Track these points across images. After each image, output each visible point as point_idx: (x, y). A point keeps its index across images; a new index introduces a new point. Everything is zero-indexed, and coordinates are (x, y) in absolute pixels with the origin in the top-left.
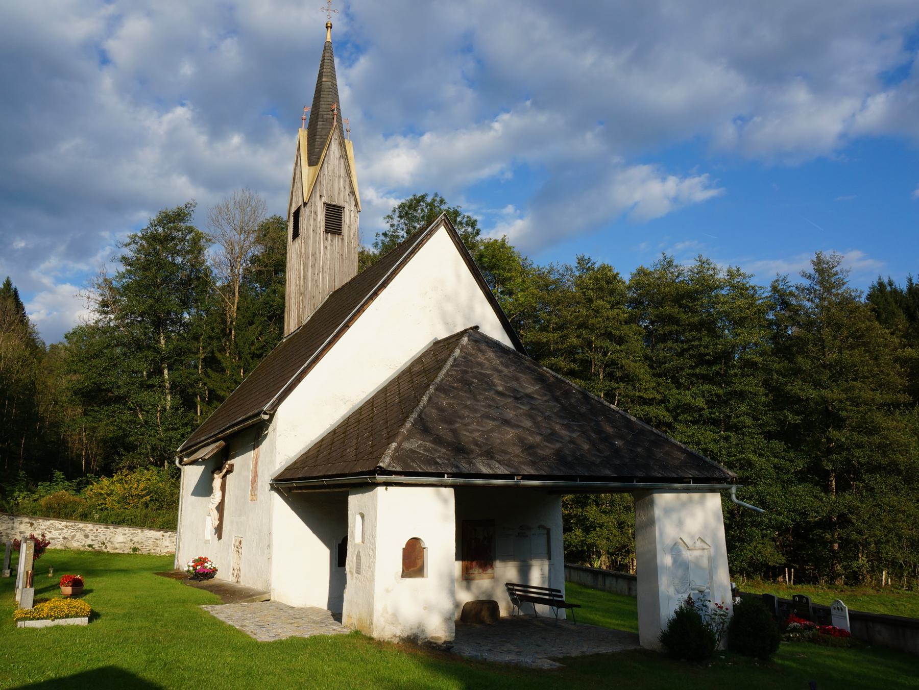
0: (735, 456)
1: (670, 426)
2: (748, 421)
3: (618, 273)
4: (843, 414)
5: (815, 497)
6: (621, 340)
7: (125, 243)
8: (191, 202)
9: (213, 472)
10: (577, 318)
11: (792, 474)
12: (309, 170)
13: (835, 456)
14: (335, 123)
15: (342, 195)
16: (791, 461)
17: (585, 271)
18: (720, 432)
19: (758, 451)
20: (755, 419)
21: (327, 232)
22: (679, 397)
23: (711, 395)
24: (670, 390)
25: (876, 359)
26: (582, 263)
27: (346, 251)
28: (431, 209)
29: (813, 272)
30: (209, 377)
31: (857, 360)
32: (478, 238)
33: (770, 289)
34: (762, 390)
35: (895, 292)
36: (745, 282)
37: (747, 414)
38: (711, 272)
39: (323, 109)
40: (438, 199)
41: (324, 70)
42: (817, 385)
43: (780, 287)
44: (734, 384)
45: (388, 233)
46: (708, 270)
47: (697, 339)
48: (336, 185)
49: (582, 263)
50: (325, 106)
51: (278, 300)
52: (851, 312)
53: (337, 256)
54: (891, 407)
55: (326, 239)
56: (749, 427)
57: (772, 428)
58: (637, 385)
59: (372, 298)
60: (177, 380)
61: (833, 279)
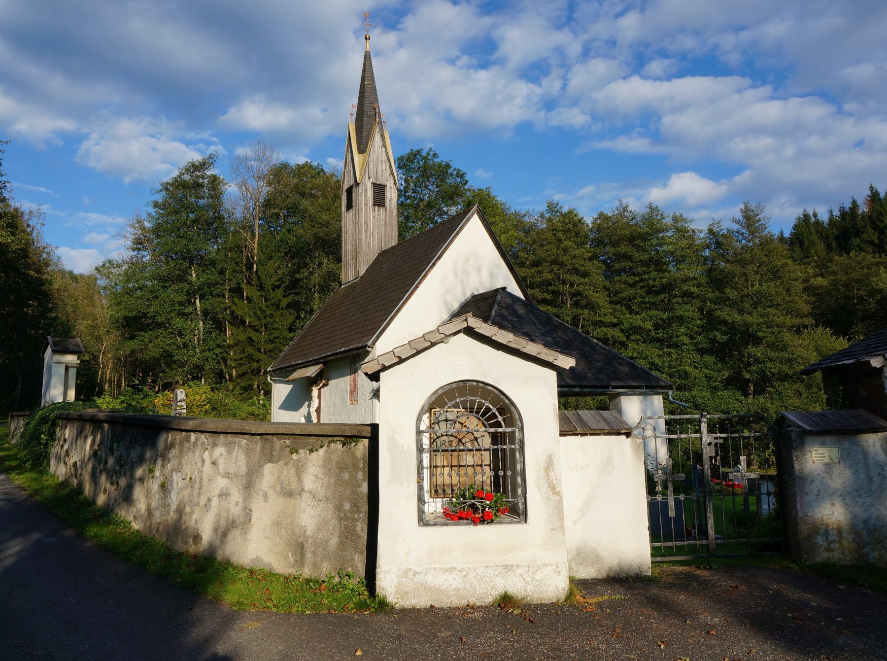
0: (675, 368)
1: (623, 344)
2: (686, 340)
3: (582, 218)
4: (760, 334)
5: (737, 400)
6: (585, 275)
7: (158, 189)
8: (214, 153)
9: (312, 386)
10: (549, 256)
11: (719, 382)
12: (359, 157)
13: (753, 368)
14: (377, 119)
15: (385, 175)
16: (719, 371)
17: (553, 213)
18: (664, 349)
19: (693, 364)
20: (692, 338)
21: (374, 205)
22: (631, 321)
23: (657, 319)
24: (624, 315)
25: (788, 290)
26: (552, 207)
27: (389, 219)
28: (425, 162)
29: (741, 219)
30: (235, 304)
31: (773, 291)
32: (466, 187)
33: (707, 231)
34: (697, 315)
35: (818, 223)
36: (687, 226)
37: (686, 335)
38: (659, 217)
39: (367, 107)
40: (432, 153)
41: (366, 75)
42: (741, 312)
43: (715, 229)
44: (676, 310)
46: (657, 215)
47: (647, 273)
48: (380, 168)
49: (552, 207)
50: (369, 105)
51: (527, 329)
52: (770, 252)
53: (382, 223)
54: (798, 330)
55: (374, 210)
56: (686, 345)
57: (705, 346)
58: (598, 311)
59: (432, 267)
60: (209, 308)
61: (757, 225)
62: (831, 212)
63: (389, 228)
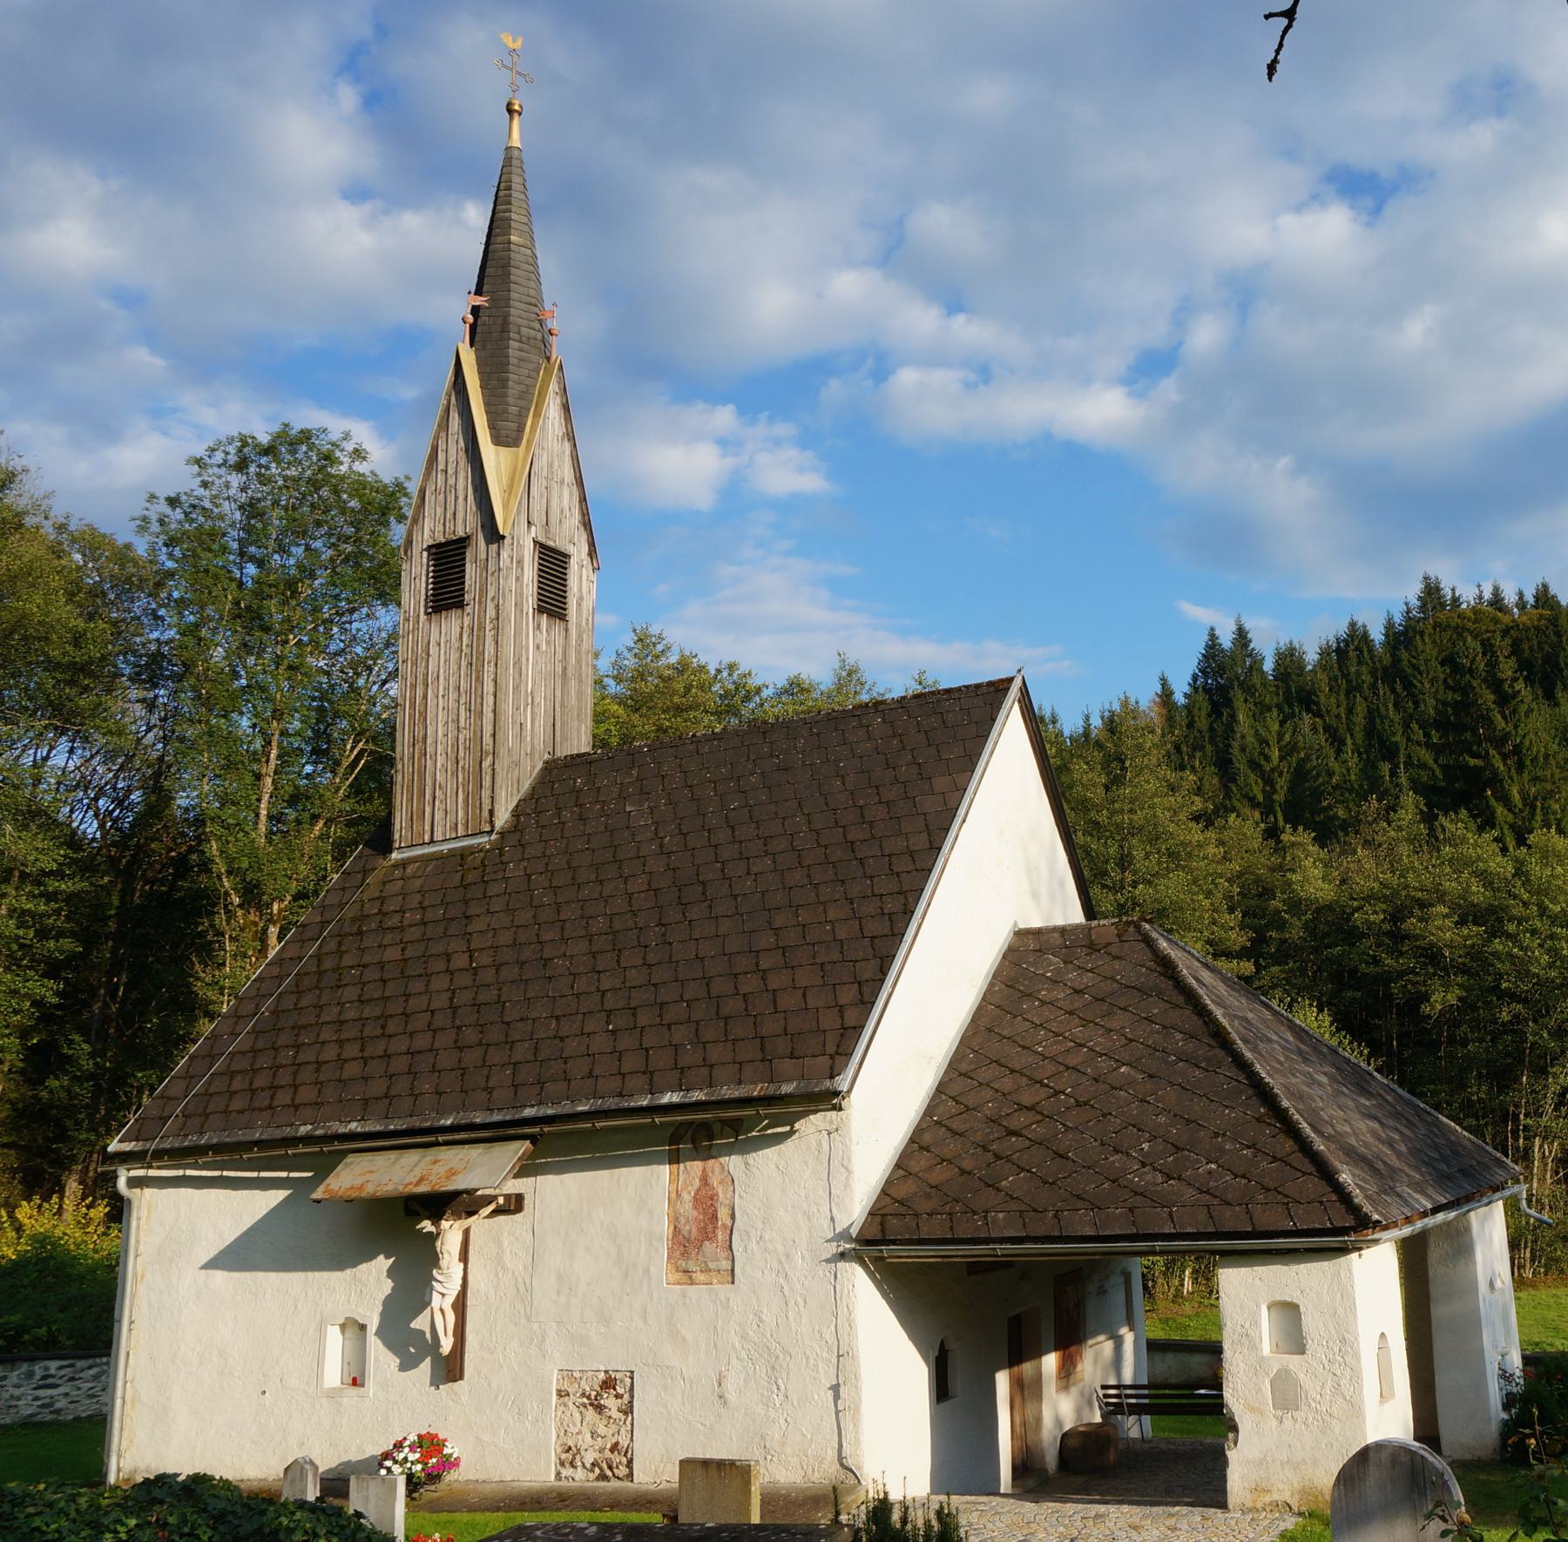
12: (497, 454)
15: (566, 526)
21: (540, 610)
45: (184, 498)
62: (1087, 718)
63: (573, 684)
